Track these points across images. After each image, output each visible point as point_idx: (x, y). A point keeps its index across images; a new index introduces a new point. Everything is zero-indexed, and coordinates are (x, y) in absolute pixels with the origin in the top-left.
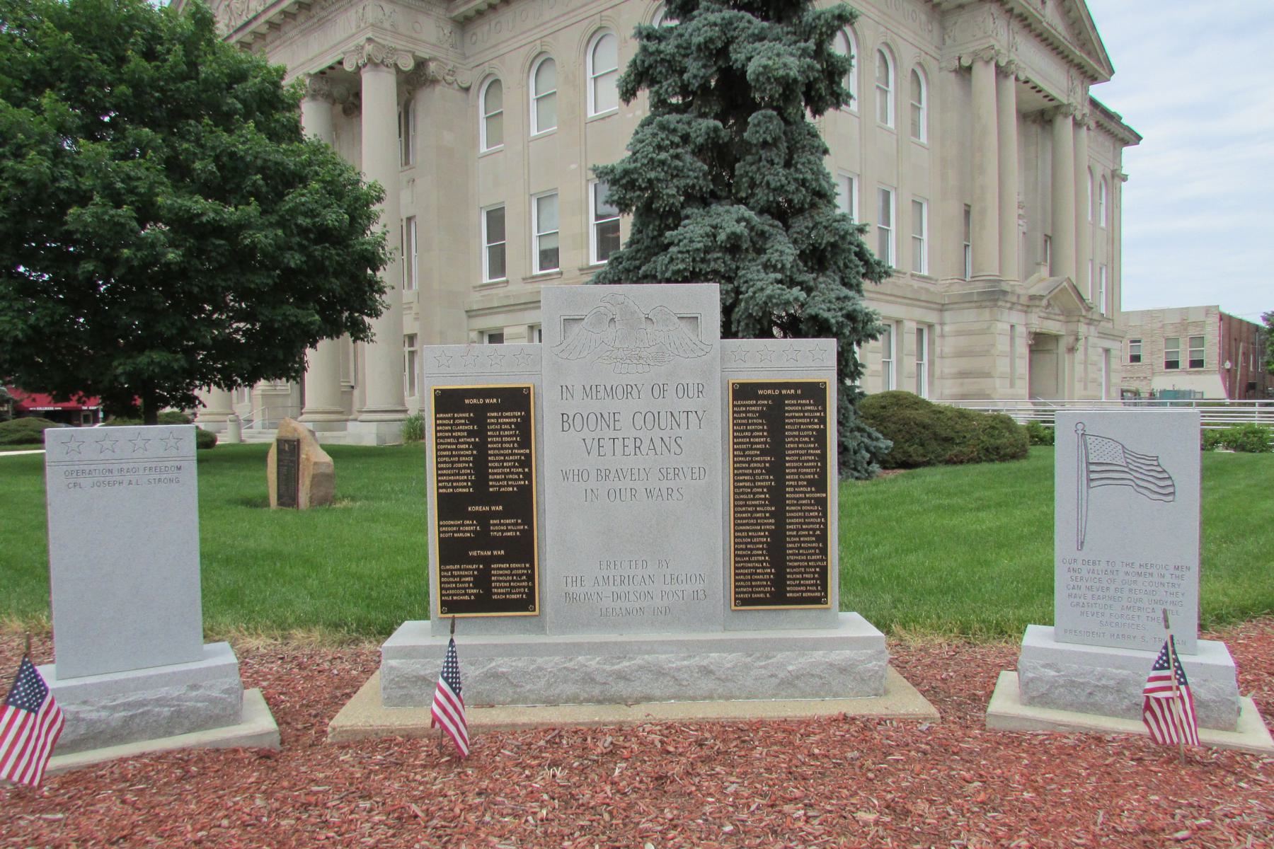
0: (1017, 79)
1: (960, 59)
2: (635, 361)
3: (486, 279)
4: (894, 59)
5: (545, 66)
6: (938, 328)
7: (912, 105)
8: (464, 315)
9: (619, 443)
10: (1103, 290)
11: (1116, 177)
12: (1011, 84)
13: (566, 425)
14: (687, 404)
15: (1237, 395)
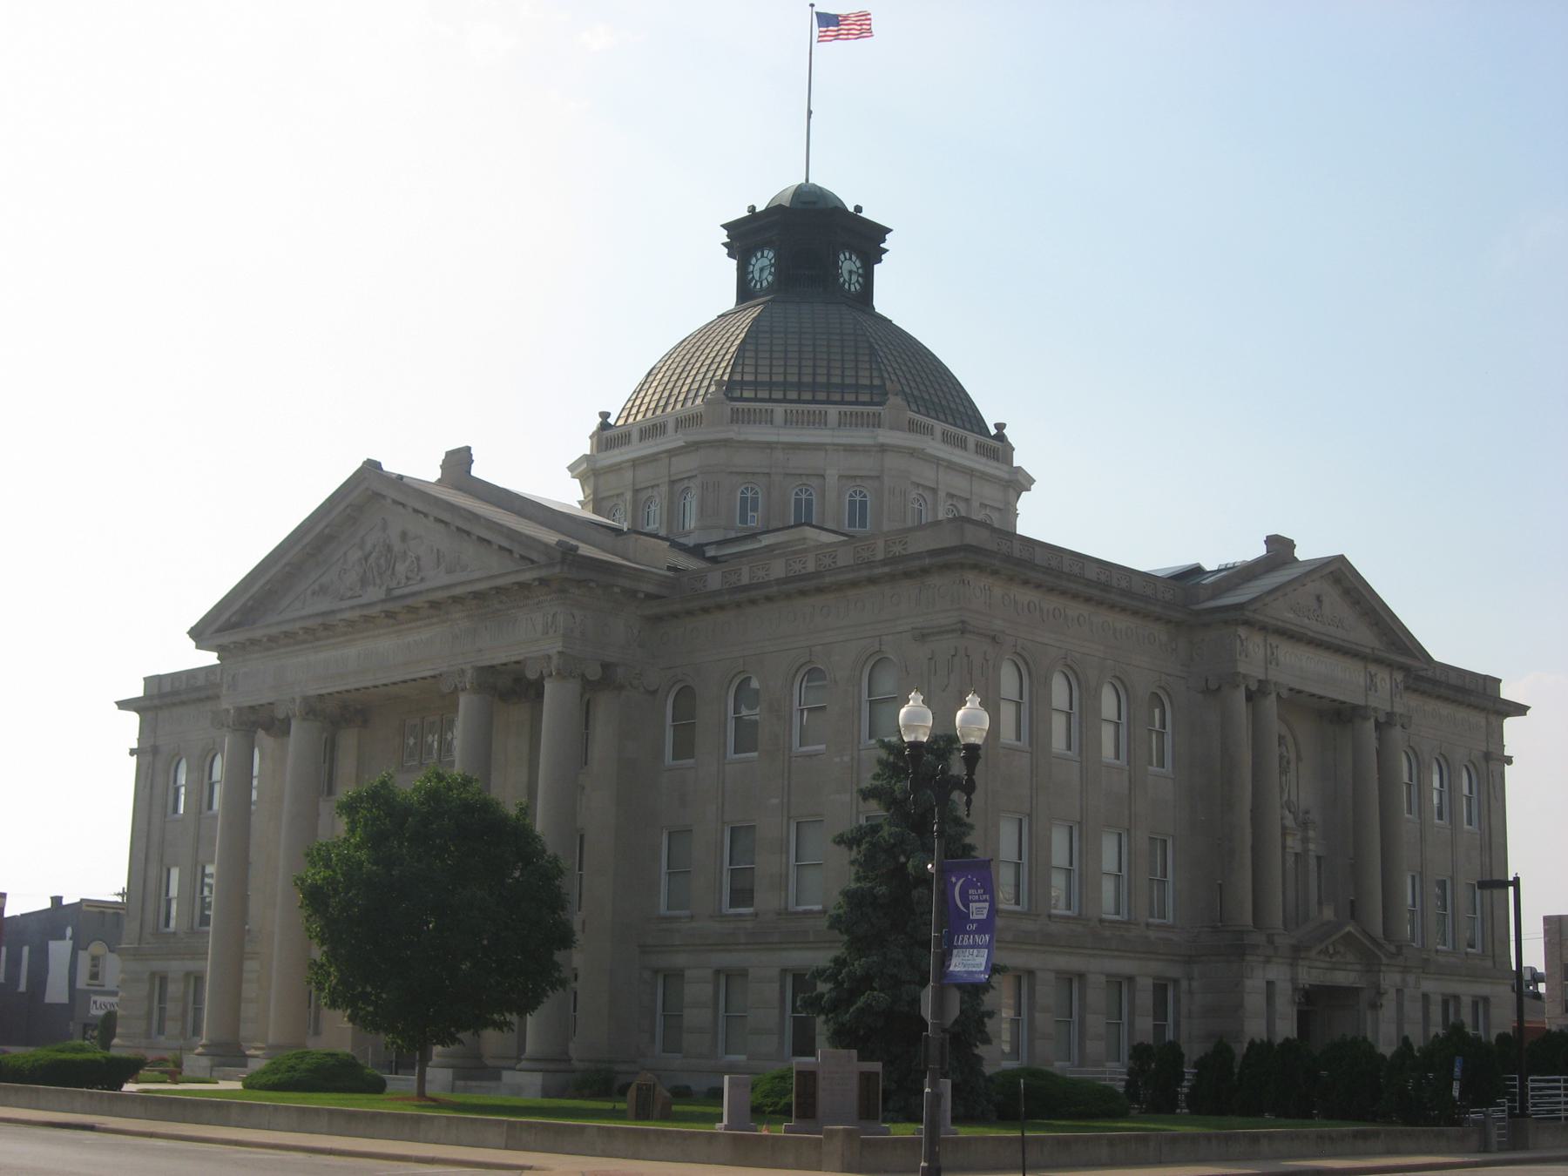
6: (1184, 984)
15: (717, 1110)
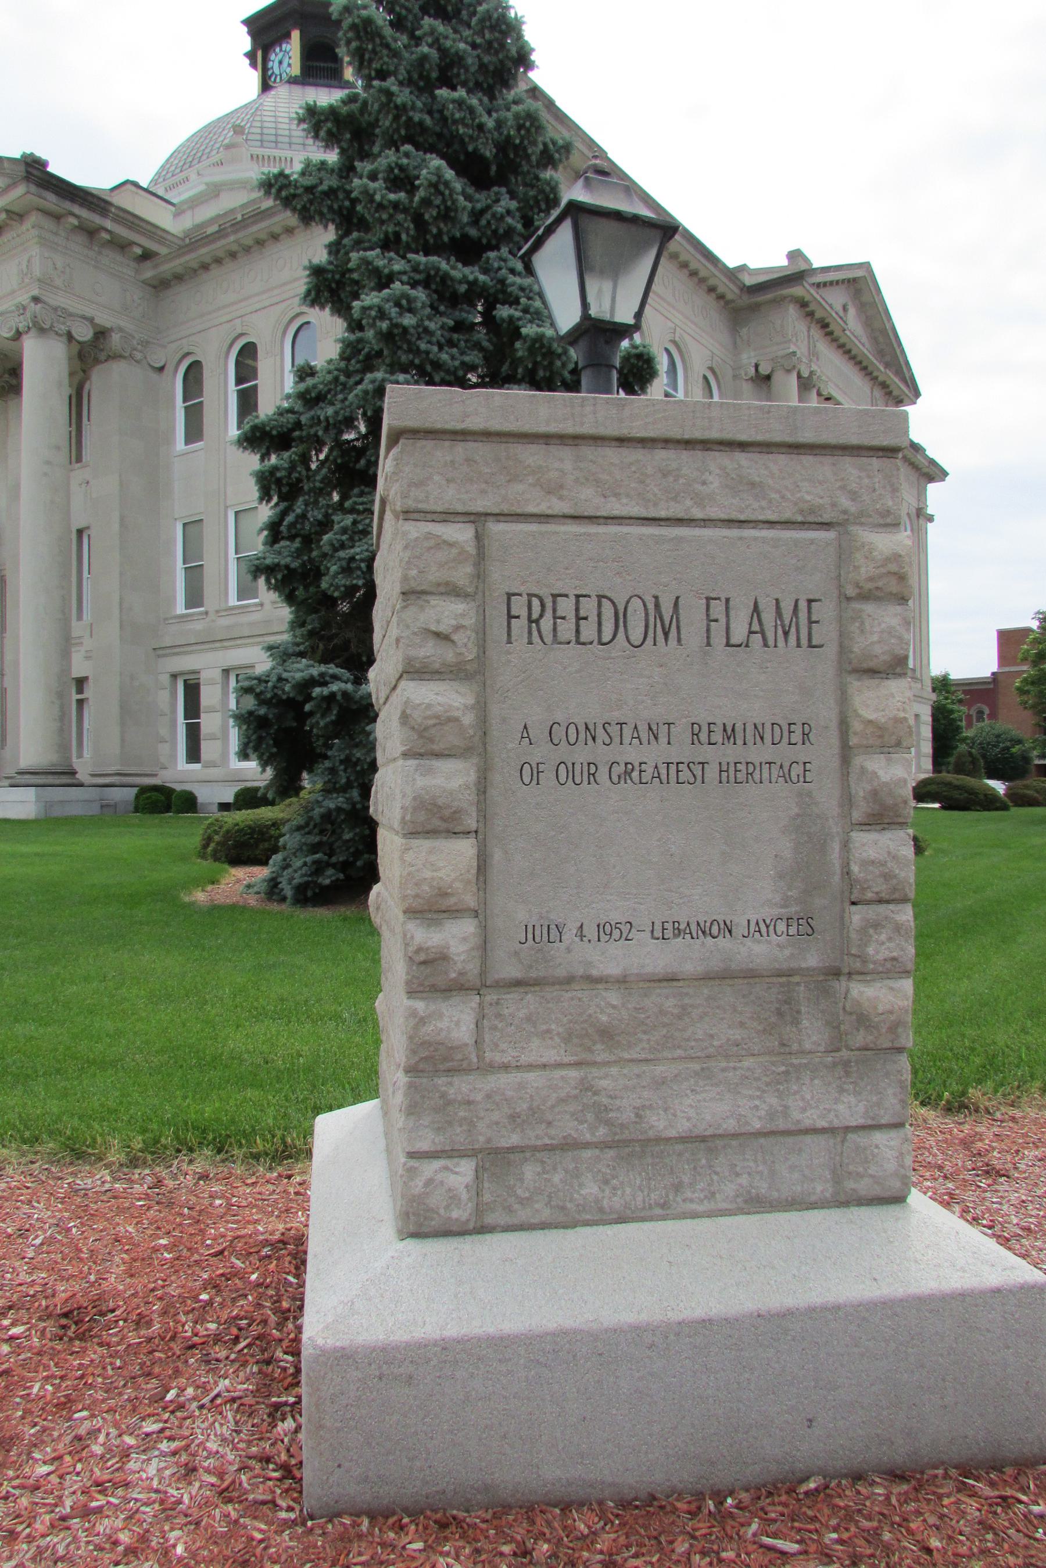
3: (233, 601)
5: (301, 334)
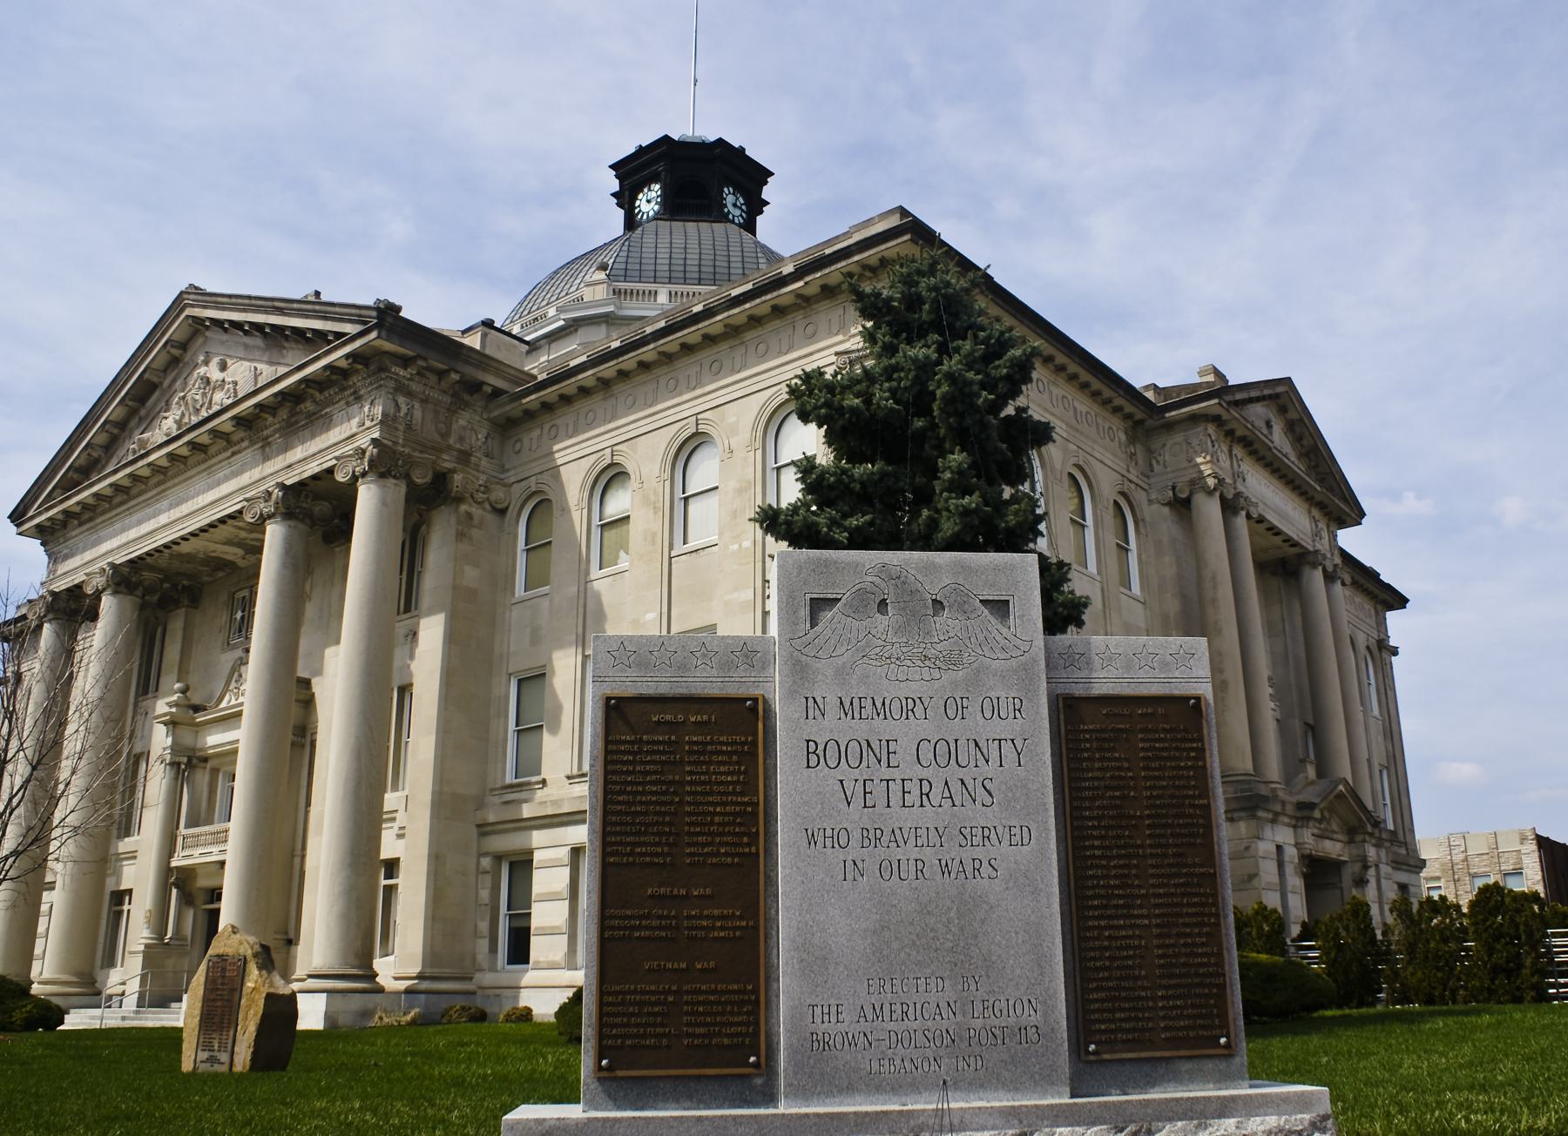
0: (1249, 516)
1: (1174, 488)
2: (919, 663)
4: (1090, 486)
7: (1118, 545)
8: (474, 831)
9: (895, 788)
10: (1388, 801)
11: (1383, 650)
12: (1241, 521)
13: (813, 758)
14: (999, 728)
